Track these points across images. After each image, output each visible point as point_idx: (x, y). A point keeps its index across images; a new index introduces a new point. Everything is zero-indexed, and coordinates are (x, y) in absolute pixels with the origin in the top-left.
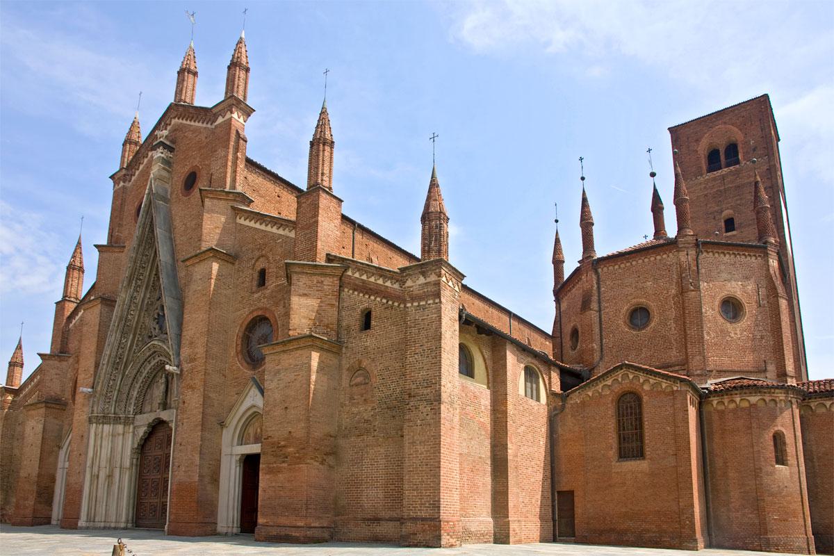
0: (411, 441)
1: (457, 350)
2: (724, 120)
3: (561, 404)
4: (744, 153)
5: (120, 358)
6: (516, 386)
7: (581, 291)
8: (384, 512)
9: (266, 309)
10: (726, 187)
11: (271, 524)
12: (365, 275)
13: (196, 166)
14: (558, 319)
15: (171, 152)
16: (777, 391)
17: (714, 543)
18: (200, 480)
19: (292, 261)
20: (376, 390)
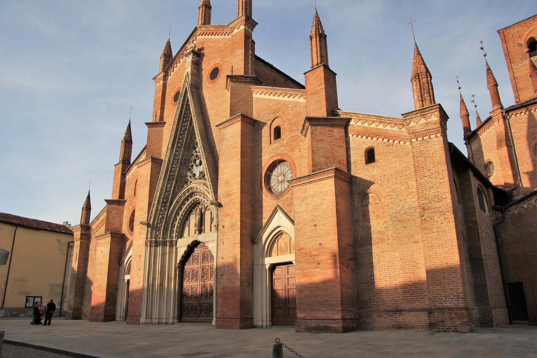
0: (429, 245)
3: (501, 215)
5: (166, 199)
9: (284, 154)
11: (309, 317)
12: (366, 123)
13: (218, 63)
15: (198, 57)
18: (241, 285)
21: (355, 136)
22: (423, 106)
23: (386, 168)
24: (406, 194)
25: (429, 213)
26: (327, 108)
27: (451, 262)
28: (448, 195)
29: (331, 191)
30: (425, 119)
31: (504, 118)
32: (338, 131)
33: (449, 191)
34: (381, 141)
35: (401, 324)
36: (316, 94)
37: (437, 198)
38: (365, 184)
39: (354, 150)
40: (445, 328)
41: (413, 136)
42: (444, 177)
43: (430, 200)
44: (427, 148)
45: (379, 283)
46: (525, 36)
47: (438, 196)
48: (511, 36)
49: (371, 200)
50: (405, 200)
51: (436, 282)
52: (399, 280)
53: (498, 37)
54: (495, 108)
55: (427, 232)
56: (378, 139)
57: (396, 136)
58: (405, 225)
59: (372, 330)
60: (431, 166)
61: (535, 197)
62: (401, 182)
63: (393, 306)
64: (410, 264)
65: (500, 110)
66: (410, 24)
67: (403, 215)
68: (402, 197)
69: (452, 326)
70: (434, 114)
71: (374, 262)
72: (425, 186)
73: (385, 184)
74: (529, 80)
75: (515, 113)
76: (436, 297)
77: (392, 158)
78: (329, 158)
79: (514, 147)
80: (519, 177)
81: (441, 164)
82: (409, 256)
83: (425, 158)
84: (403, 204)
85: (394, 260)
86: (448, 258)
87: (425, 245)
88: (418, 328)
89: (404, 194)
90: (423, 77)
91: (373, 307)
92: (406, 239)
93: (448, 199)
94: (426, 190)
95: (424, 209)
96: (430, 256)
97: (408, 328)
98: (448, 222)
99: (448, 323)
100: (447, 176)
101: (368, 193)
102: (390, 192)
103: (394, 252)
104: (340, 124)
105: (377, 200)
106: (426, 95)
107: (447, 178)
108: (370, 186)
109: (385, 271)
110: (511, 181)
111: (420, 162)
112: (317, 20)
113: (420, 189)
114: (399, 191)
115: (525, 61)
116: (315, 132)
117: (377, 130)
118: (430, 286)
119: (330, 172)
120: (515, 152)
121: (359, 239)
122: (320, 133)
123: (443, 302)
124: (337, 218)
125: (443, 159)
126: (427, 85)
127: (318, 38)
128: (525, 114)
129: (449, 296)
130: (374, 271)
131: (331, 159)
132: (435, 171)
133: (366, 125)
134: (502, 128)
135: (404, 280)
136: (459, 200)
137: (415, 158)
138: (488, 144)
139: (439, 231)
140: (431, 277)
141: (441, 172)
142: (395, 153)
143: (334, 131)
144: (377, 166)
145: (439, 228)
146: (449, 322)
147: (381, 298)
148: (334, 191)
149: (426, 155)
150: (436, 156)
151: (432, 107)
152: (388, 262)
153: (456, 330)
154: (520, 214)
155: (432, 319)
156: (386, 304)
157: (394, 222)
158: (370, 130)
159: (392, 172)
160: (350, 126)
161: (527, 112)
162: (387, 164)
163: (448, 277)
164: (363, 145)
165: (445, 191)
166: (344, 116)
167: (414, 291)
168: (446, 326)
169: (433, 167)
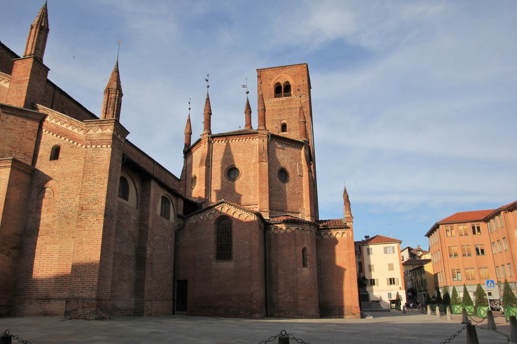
0: (79, 242)
1: (118, 180)
2: (285, 72)
3: (183, 223)
4: (294, 91)
6: (155, 209)
7: (200, 153)
8: (54, 293)
10: (284, 108)
14: (185, 169)
16: (305, 224)
17: (269, 314)
19: (30, 110)
20: (58, 203)
21: (47, 132)
22: (105, 118)
23: (65, 167)
24: (76, 193)
25: (85, 213)
26: (26, 99)
27: (93, 258)
28: (103, 199)
29: (5, 180)
30: (102, 130)
31: (209, 142)
32: (32, 124)
33: (106, 196)
34: (68, 142)
35: (47, 311)
36: (20, 83)
37: (95, 201)
38: (44, 179)
39: (44, 145)
40: (77, 315)
41: (89, 143)
42: (105, 183)
43: (89, 202)
44: (97, 156)
45: (37, 273)
46: (274, 79)
47: (96, 199)
48: (265, 77)
49: (46, 194)
50: (74, 198)
51: (78, 275)
52: (54, 271)
53: (256, 74)
54: (205, 132)
55: (80, 230)
56: (65, 139)
57: (80, 139)
58: (69, 221)
59: (21, 316)
60: (97, 172)
61: (210, 211)
62: (75, 182)
63: (44, 294)
64: (66, 257)
65: (207, 135)
66: (118, 43)
67: (70, 212)
68: (72, 196)
69: (83, 314)
70: (109, 127)
71: (36, 253)
72: (88, 189)
73: (61, 182)
74: (270, 116)
75: (218, 140)
76: (75, 288)
77: (73, 159)
78: (15, 148)
79: (211, 168)
80: (210, 193)
81: (105, 171)
82: (66, 250)
83: (94, 164)
84: (72, 202)
85: (54, 252)
86: (92, 254)
87: (76, 241)
88: (61, 315)
89: (74, 193)
90: (113, 92)
91: (27, 294)
92: (68, 234)
93: (103, 203)
94: (87, 192)
95: (82, 209)
96: (78, 251)
97: (52, 315)
98: (98, 223)
99: (80, 311)
100: (106, 183)
101: (45, 187)
102: (64, 189)
103: (55, 245)
104: (35, 118)
105: (51, 195)
106: (110, 109)
107: (106, 185)
108: (49, 181)
109: (44, 261)
110: (203, 195)
111: (89, 167)
112: (44, 12)
113: (83, 191)
114: (71, 190)
115: (271, 99)
116: (6, 120)
117: (66, 131)
118: (73, 278)
119: (8, 162)
120: (211, 171)
121: (29, 230)
122: (11, 122)
123: (80, 293)
124: (4, 207)
125: (107, 167)
126: (113, 100)
127: (38, 29)
128: (225, 142)
129: (86, 288)
130: (35, 261)
131: (17, 149)
132: (98, 177)
133: (59, 124)
134: (206, 150)
135: (58, 271)
136: (137, 205)
137: (86, 162)
138: (197, 161)
139: (90, 230)
140: (75, 270)
141: (103, 178)
142: (76, 155)
143: (27, 123)
144: (58, 163)
145: (90, 227)
146: (80, 310)
147: (35, 286)
148: (8, 180)
149: (95, 162)
150: (103, 164)
151: (109, 121)
152: (48, 254)
153: (85, 317)
154: (197, 223)
155: (68, 307)
156: (39, 292)
157: (60, 217)
158: (61, 129)
159: (69, 171)
160: (45, 122)
161: (226, 141)
162: (67, 164)
163: (89, 271)
164: (52, 142)
165: (102, 196)
166: (42, 111)
167: (64, 281)
168: (78, 314)
169: (98, 173)
